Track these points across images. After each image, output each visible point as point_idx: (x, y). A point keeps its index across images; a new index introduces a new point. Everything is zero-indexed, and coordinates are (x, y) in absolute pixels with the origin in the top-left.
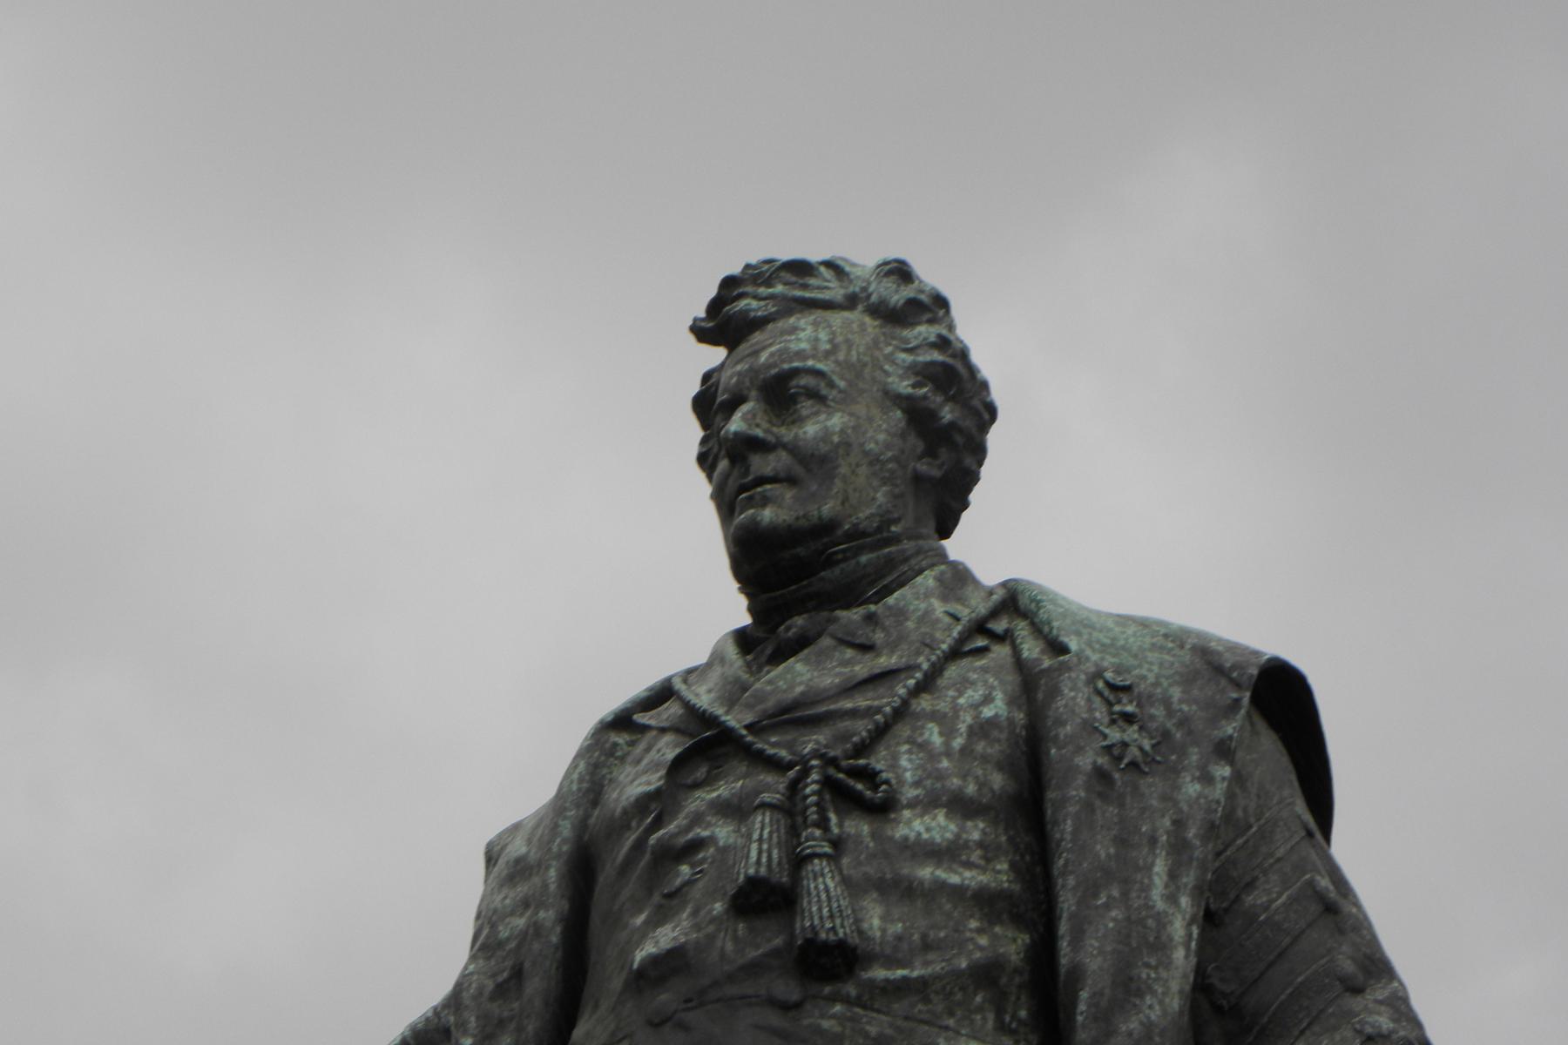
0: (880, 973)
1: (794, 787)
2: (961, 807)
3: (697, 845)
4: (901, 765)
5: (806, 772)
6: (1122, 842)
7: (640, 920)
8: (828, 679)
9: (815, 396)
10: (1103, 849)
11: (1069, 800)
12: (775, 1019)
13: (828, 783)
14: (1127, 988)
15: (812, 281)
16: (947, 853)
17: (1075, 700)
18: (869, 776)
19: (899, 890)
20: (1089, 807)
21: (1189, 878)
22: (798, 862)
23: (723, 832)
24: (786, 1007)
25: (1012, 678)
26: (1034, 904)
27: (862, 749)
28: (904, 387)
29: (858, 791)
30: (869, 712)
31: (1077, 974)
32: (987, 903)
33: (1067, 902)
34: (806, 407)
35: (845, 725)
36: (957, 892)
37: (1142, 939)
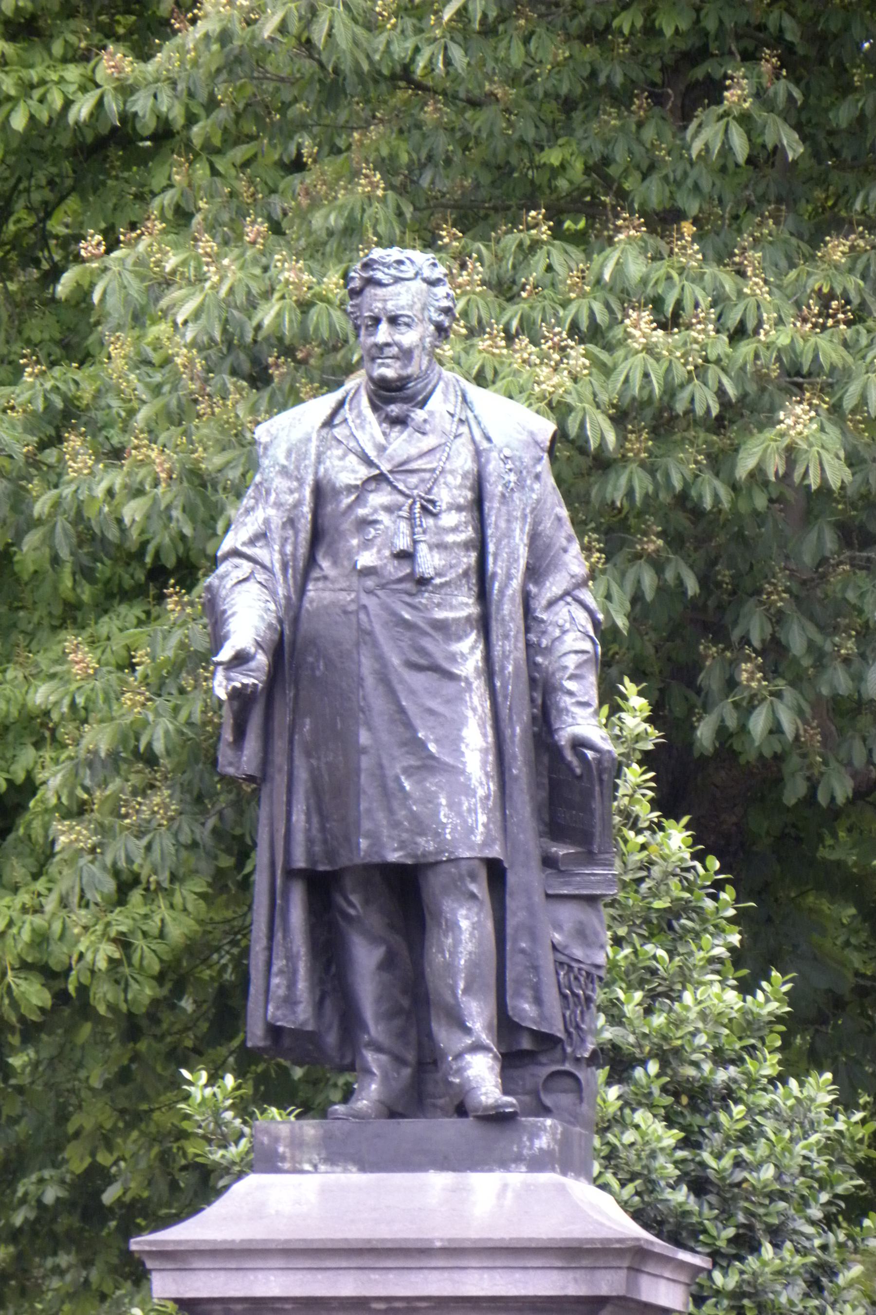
0: (437, 581)
1: (411, 508)
2: (459, 508)
3: (376, 522)
4: (443, 496)
5: (414, 503)
6: (508, 521)
7: (355, 542)
8: (413, 451)
9: (408, 325)
10: (503, 524)
11: (492, 507)
12: (408, 599)
13: (424, 508)
14: (509, 577)
15: (403, 268)
16: (455, 530)
17: (494, 467)
18: (433, 502)
19: (441, 546)
20: (499, 509)
21: (527, 528)
22: (415, 542)
23: (383, 516)
24: (410, 595)
25: (471, 448)
26: (480, 545)
27: (429, 491)
28: (436, 317)
29: (429, 509)
30: (433, 470)
31: (494, 574)
32: (467, 546)
33: (491, 548)
34: (403, 329)
35: (423, 475)
36: (455, 544)
37: (513, 559)
